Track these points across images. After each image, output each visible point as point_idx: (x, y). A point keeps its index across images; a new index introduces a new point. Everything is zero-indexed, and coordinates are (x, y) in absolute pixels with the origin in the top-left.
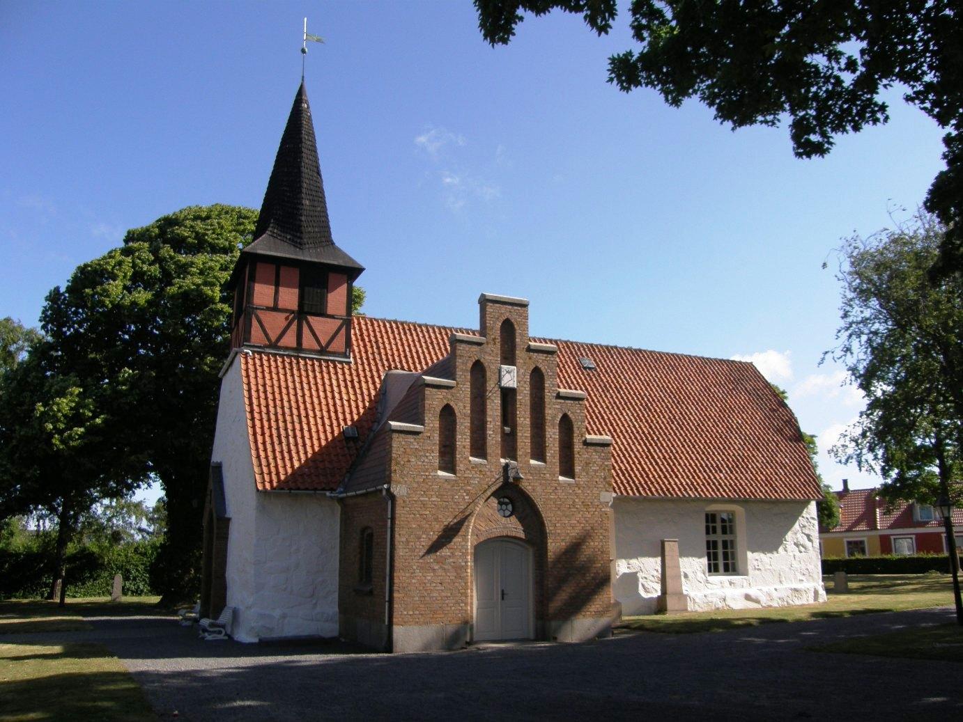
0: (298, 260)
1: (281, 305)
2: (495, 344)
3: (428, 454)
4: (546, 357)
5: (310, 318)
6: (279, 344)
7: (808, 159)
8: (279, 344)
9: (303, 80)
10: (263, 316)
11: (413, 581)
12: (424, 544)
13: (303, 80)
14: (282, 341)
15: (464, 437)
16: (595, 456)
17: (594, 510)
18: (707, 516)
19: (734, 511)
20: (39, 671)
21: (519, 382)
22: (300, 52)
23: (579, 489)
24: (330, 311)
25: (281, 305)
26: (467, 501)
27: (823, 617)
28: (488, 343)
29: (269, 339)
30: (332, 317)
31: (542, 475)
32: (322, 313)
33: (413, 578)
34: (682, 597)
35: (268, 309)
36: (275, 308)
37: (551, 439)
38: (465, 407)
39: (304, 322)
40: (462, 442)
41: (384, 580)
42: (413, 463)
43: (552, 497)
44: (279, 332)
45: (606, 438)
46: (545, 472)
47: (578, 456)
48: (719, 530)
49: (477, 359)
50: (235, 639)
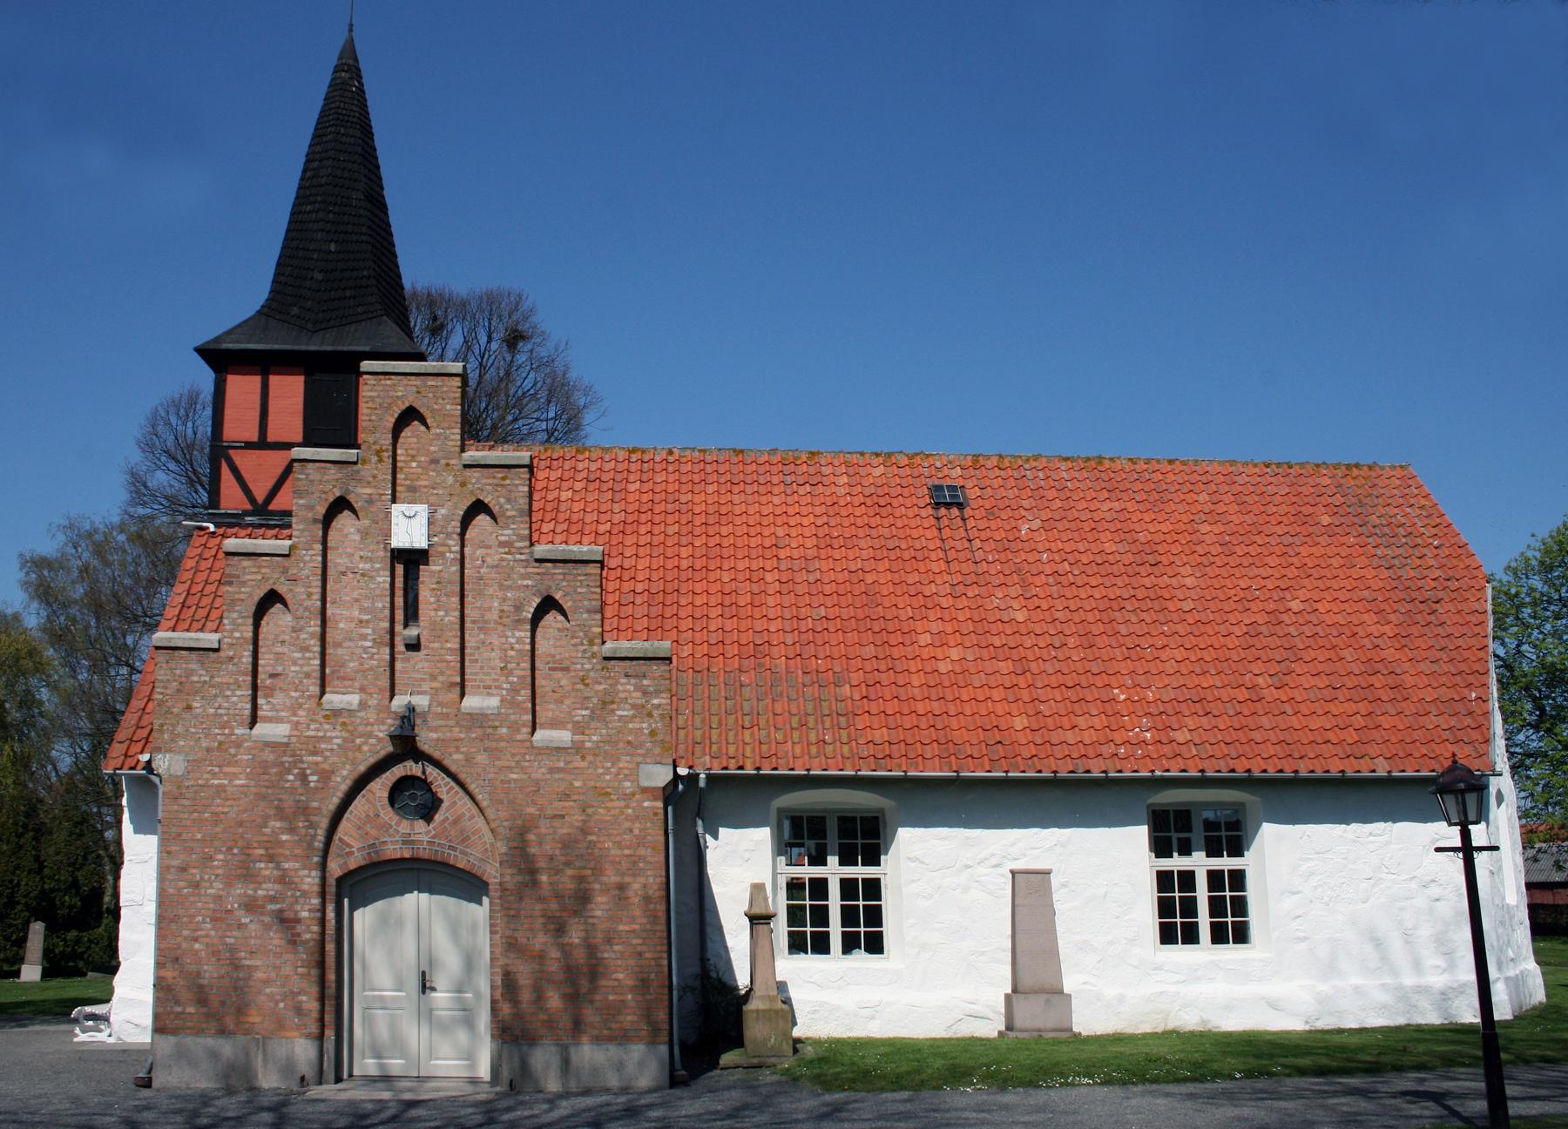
1: (271, 438)
2: (381, 460)
3: (228, 693)
4: (503, 479)
6: (271, 507)
8: (271, 507)
9: (351, 30)
10: (243, 460)
11: (197, 946)
12: (220, 871)
13: (351, 30)
14: (275, 501)
15: (307, 655)
16: (626, 687)
23: (583, 758)
25: (271, 438)
27: (1465, 1123)
29: (252, 500)
35: (249, 445)
36: (262, 444)
37: (512, 653)
38: (310, 595)
40: (302, 666)
41: (677, 906)
43: (514, 776)
44: (270, 484)
46: (497, 724)
49: (338, 494)
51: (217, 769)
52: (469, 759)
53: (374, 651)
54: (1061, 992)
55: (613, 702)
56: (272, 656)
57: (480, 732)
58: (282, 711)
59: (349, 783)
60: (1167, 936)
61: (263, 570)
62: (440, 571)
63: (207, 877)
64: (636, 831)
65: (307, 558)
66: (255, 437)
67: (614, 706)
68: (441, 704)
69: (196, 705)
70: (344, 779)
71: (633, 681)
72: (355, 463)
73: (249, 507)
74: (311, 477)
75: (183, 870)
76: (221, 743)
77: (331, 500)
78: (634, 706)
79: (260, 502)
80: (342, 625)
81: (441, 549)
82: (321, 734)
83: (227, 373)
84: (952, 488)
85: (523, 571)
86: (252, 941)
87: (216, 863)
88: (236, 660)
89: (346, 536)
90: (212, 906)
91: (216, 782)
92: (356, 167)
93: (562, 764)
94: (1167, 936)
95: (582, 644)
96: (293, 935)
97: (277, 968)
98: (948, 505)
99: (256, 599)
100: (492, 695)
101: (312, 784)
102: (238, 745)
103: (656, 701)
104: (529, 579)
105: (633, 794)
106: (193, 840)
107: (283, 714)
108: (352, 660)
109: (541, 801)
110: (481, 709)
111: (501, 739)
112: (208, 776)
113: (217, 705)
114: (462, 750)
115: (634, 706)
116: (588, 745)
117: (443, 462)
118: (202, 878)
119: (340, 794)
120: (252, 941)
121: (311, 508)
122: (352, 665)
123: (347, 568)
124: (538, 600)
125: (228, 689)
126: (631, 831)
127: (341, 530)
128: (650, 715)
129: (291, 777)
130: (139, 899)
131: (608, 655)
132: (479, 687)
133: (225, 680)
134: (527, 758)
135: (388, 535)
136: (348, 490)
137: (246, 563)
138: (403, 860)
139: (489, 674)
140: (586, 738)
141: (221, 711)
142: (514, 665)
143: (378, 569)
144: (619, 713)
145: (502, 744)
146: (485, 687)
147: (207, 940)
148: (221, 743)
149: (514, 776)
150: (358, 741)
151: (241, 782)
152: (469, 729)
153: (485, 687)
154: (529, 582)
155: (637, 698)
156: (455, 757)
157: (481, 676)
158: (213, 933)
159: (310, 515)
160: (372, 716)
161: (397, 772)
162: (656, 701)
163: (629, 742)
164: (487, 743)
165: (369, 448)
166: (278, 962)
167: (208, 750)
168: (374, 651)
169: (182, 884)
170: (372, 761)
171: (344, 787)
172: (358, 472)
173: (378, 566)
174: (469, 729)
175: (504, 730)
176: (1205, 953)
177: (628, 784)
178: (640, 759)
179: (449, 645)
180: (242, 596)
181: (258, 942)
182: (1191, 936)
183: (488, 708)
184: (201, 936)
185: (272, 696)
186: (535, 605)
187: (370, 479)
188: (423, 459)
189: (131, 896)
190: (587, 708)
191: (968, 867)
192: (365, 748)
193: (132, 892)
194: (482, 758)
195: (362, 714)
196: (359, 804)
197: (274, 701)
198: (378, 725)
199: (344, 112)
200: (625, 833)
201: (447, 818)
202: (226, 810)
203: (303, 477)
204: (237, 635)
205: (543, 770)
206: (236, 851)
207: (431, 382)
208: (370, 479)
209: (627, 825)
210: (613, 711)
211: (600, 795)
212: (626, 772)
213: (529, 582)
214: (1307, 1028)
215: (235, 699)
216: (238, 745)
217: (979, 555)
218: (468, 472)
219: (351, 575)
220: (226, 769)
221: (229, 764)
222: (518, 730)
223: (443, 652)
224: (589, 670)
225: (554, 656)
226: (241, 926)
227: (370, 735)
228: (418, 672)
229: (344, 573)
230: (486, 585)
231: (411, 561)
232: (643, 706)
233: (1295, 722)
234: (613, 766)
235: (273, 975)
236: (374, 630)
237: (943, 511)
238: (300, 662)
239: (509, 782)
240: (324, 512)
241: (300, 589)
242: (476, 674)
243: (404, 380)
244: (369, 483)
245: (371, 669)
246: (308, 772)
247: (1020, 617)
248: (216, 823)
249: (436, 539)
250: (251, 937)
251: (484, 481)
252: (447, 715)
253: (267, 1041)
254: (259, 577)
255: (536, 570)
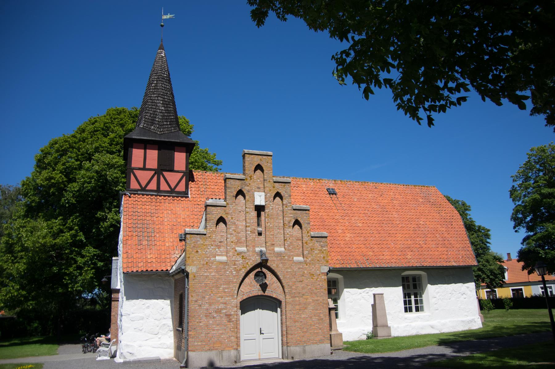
0: (156, 140)
1: (147, 167)
3: (209, 247)
5: (165, 173)
7: (545, 122)
8: (147, 189)
10: (137, 172)
15: (232, 236)
16: (317, 244)
17: (317, 277)
18: (402, 277)
19: (421, 275)
20: (479, 326)
21: (266, 202)
22: (161, 27)
23: (307, 265)
24: (176, 168)
25: (147, 167)
26: (234, 274)
28: (246, 179)
30: (178, 172)
31: (283, 258)
32: (172, 170)
33: (200, 322)
34: (386, 326)
35: (140, 169)
36: (144, 169)
37: (288, 235)
39: (161, 176)
40: (231, 239)
42: (200, 253)
45: (325, 234)
46: (284, 255)
47: (305, 245)
48: (411, 287)
49: (240, 189)
50: (116, 362)
51: (206, 270)
52: (277, 266)
53: (251, 235)
54: (387, 326)
55: (314, 249)
56: (220, 236)
57: (280, 258)
58: (223, 252)
59: (245, 273)
60: (406, 311)
61: (218, 211)
62: (268, 212)
63: (203, 303)
64: (320, 285)
65: (231, 207)
66: (142, 167)
67: (314, 250)
68: (269, 250)
69: (199, 251)
70: (243, 272)
71: (318, 243)
72: (244, 180)
73: (140, 188)
74: (232, 183)
75: (196, 301)
76: (207, 262)
77: (238, 190)
78: (319, 250)
79: (173, 188)
80: (240, 227)
81: (268, 206)
82: (236, 259)
83: (132, 148)
84: (332, 189)
85: (290, 212)
86: (217, 322)
87: (206, 299)
88: (211, 238)
89: (240, 201)
90: (205, 312)
91: (206, 274)
92: (167, 84)
93: (301, 267)
94: (406, 311)
95: (306, 233)
96: (229, 319)
97: (225, 330)
98: (333, 194)
99: (217, 219)
100: (281, 247)
101: (234, 274)
102: (212, 263)
103: (324, 249)
104: (292, 214)
105: (319, 275)
106: (199, 292)
107: (223, 253)
108: (243, 237)
109: (296, 277)
110: (280, 251)
111: (286, 260)
112: (203, 272)
113: (206, 251)
114: (276, 263)
115: (319, 250)
116: (308, 261)
117: (268, 180)
118: (202, 304)
119: (242, 277)
120: (217, 322)
121: (232, 192)
122: (243, 239)
123: (241, 210)
124: (294, 220)
125: (209, 246)
126: (319, 285)
127: (239, 199)
128: (323, 252)
129: (228, 272)
130: (129, 313)
131: (313, 236)
132: (278, 245)
133: (208, 244)
134: (293, 265)
135: (254, 201)
136: (242, 187)
137: (213, 208)
138: (258, 296)
139: (280, 241)
140: (307, 259)
141: (207, 253)
142: (288, 239)
143: (251, 211)
144: (315, 252)
145: (286, 261)
146: (279, 245)
147: (204, 322)
148: (207, 262)
149: (289, 270)
150: (247, 261)
151: (213, 274)
152: (277, 257)
153: (280, 245)
154: (292, 215)
155: (320, 248)
156: (274, 265)
157: (278, 242)
158: (206, 320)
159: (232, 195)
160: (251, 254)
161: (259, 270)
162: (324, 249)
163: (318, 260)
164: (282, 261)
165: (248, 175)
166: (225, 328)
167: (203, 265)
168: (251, 235)
169: (196, 306)
170: (251, 267)
171: (243, 275)
172: (245, 182)
173: (251, 210)
174: (277, 257)
175: (286, 257)
176: (414, 315)
177: (318, 272)
178: (321, 265)
179: (271, 233)
180: (213, 218)
181: (219, 322)
182: (411, 310)
183: (282, 251)
184: (202, 321)
185: (220, 248)
186: (293, 222)
187: (248, 184)
188: (261, 179)
189: (126, 312)
190: (307, 251)
191: (361, 293)
192: (249, 263)
193: (127, 311)
194: (281, 265)
195: (248, 253)
196: (247, 280)
197: (221, 250)
198: (253, 256)
199: (158, 68)
200: (317, 285)
201: (270, 283)
202: (209, 283)
203: (229, 183)
204: (211, 230)
205: (297, 268)
206: (212, 295)
207: (264, 157)
208: (248, 184)
209: (318, 283)
210: (314, 251)
211: (311, 275)
212: (318, 268)
213: (292, 215)
214: (439, 332)
215: (211, 249)
216: (212, 263)
217: (345, 208)
218: (275, 184)
219: (242, 212)
220: (209, 270)
221: (210, 269)
222: (290, 257)
223: (270, 235)
224: (307, 240)
225: (297, 236)
226: (214, 317)
227: (250, 259)
228: (261, 241)
229: (240, 212)
230: (279, 216)
231: (259, 209)
232: (321, 250)
233: (431, 253)
234: (314, 266)
235: (224, 332)
236: (251, 229)
237: (332, 196)
238: (230, 238)
239: (288, 272)
240: (236, 193)
241: (229, 217)
242: (277, 241)
243: (257, 156)
244: (248, 186)
245: (250, 240)
246: (233, 271)
247: (360, 225)
248: (206, 287)
249: (267, 203)
250: (217, 321)
251: (279, 186)
252: (271, 253)
253: (223, 351)
254: (217, 212)
255: (293, 212)
